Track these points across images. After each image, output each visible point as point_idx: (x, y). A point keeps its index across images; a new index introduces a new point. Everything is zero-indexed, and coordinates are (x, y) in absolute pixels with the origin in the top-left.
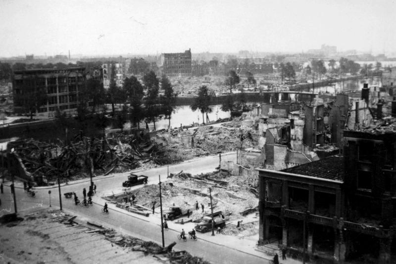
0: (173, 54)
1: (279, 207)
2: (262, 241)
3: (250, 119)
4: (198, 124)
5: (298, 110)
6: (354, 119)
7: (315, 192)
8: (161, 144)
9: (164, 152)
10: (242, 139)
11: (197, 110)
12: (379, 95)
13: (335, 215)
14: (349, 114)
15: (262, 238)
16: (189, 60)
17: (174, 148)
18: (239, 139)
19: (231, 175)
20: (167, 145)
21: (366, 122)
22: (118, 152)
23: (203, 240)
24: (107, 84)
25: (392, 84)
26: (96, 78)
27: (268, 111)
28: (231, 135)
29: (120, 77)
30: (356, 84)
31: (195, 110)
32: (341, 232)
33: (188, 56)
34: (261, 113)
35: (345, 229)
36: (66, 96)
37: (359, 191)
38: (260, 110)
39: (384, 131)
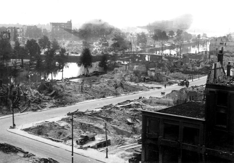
0: (59, 23)
3: (120, 73)
6: (213, 76)
8: (60, 90)
9: (63, 96)
10: (116, 88)
12: (209, 57)
13: (198, 144)
14: (210, 71)
17: (69, 93)
18: (113, 88)
20: (64, 91)
21: (220, 78)
22: (29, 95)
23: (19, 148)
24: (12, 43)
25: (217, 49)
26: (5, 39)
28: (108, 85)
29: (21, 39)
30: (189, 48)
32: (203, 156)
34: (128, 69)
35: (207, 154)
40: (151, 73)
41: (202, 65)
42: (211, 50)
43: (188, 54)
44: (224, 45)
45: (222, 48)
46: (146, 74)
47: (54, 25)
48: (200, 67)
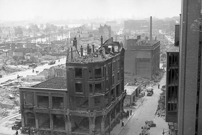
1: (32, 107)
5: (29, 52)
21: (76, 58)
25: (76, 36)
27: (13, 54)
32: (68, 116)
34: (8, 55)
35: (70, 115)
37: (76, 94)
38: (8, 54)
39: (88, 62)
40: (27, 57)
41: (65, 49)
44: (80, 33)
45: (79, 35)
46: (24, 58)
48: (64, 50)
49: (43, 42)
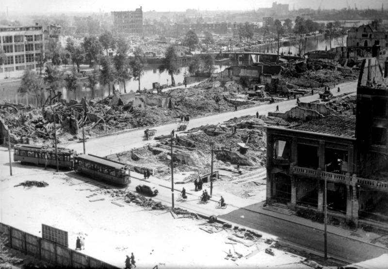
2: (270, 200)
4: (167, 86)
7: (326, 149)
11: (165, 72)
12: (348, 56)
15: (269, 197)
16: (140, 19)
19: (267, 203)
25: (358, 44)
27: (240, 72)
31: (163, 72)
32: (354, 188)
33: (139, 15)
34: (232, 74)
36: (23, 56)
42: (349, 46)
43: (316, 51)
47: (118, 15)
49: (291, 54)
